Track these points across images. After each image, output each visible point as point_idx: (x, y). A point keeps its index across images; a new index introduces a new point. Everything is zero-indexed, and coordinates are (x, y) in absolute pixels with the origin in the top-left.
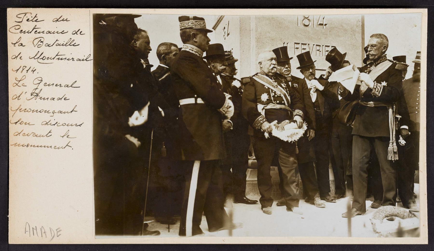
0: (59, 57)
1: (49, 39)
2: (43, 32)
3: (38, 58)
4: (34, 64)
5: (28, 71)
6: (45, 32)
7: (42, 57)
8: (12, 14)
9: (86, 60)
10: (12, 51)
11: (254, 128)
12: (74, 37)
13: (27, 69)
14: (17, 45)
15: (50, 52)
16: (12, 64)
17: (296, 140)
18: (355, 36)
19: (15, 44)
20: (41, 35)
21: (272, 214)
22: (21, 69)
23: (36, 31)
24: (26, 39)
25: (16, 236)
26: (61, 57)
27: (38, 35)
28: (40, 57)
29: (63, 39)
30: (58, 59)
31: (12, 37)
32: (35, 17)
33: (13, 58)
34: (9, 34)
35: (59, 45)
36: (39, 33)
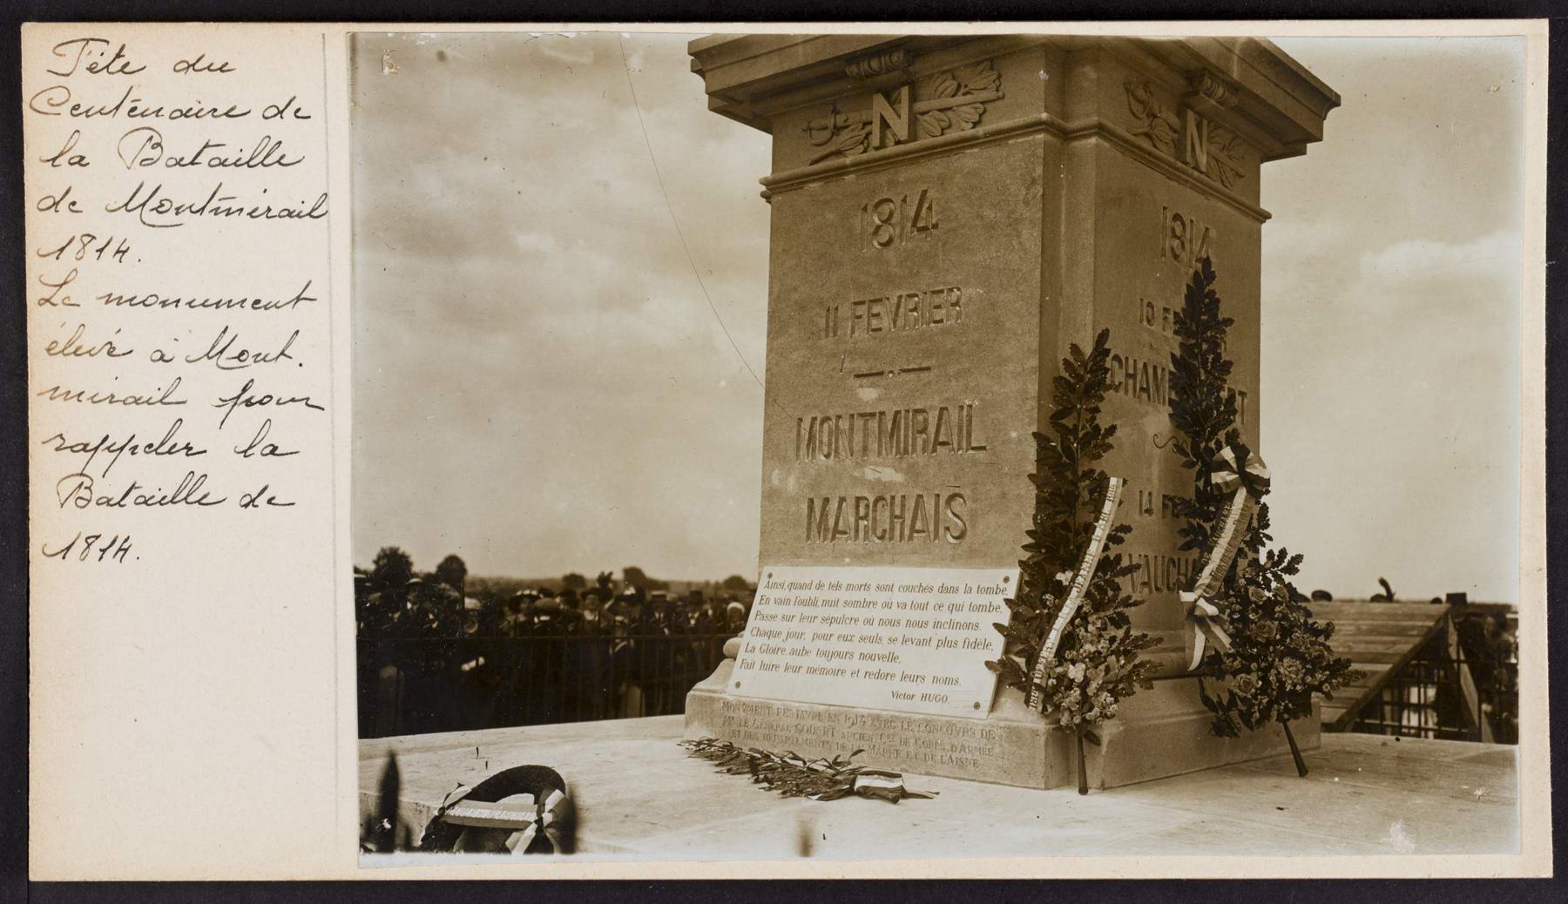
0: (216, 207)
1: (182, 138)
2: (157, 112)
3: (143, 205)
4: (125, 227)
5: (101, 250)
6: (166, 112)
7: (154, 203)
8: (44, 47)
9: (309, 214)
10: (38, 181)
11: (1201, 556)
12: (277, 128)
13: (99, 243)
14: (63, 160)
15: (189, 186)
16: (41, 231)
17: (1470, 599)
18: (1019, 236)
19: (54, 159)
20: (151, 121)
21: (1343, 102)
22: (77, 245)
23: (134, 109)
24: (99, 137)
25: (49, 861)
26: (224, 205)
27: (139, 122)
28: (148, 205)
29: (239, 138)
30: (216, 211)
31: (41, 134)
32: (118, 56)
33: (44, 205)
34: (29, 116)
35: (222, 164)
36: (142, 115)
